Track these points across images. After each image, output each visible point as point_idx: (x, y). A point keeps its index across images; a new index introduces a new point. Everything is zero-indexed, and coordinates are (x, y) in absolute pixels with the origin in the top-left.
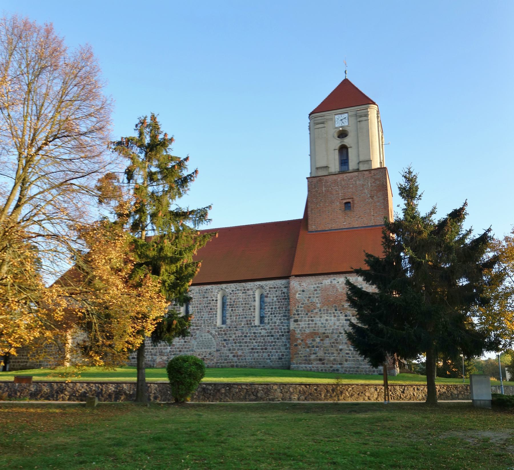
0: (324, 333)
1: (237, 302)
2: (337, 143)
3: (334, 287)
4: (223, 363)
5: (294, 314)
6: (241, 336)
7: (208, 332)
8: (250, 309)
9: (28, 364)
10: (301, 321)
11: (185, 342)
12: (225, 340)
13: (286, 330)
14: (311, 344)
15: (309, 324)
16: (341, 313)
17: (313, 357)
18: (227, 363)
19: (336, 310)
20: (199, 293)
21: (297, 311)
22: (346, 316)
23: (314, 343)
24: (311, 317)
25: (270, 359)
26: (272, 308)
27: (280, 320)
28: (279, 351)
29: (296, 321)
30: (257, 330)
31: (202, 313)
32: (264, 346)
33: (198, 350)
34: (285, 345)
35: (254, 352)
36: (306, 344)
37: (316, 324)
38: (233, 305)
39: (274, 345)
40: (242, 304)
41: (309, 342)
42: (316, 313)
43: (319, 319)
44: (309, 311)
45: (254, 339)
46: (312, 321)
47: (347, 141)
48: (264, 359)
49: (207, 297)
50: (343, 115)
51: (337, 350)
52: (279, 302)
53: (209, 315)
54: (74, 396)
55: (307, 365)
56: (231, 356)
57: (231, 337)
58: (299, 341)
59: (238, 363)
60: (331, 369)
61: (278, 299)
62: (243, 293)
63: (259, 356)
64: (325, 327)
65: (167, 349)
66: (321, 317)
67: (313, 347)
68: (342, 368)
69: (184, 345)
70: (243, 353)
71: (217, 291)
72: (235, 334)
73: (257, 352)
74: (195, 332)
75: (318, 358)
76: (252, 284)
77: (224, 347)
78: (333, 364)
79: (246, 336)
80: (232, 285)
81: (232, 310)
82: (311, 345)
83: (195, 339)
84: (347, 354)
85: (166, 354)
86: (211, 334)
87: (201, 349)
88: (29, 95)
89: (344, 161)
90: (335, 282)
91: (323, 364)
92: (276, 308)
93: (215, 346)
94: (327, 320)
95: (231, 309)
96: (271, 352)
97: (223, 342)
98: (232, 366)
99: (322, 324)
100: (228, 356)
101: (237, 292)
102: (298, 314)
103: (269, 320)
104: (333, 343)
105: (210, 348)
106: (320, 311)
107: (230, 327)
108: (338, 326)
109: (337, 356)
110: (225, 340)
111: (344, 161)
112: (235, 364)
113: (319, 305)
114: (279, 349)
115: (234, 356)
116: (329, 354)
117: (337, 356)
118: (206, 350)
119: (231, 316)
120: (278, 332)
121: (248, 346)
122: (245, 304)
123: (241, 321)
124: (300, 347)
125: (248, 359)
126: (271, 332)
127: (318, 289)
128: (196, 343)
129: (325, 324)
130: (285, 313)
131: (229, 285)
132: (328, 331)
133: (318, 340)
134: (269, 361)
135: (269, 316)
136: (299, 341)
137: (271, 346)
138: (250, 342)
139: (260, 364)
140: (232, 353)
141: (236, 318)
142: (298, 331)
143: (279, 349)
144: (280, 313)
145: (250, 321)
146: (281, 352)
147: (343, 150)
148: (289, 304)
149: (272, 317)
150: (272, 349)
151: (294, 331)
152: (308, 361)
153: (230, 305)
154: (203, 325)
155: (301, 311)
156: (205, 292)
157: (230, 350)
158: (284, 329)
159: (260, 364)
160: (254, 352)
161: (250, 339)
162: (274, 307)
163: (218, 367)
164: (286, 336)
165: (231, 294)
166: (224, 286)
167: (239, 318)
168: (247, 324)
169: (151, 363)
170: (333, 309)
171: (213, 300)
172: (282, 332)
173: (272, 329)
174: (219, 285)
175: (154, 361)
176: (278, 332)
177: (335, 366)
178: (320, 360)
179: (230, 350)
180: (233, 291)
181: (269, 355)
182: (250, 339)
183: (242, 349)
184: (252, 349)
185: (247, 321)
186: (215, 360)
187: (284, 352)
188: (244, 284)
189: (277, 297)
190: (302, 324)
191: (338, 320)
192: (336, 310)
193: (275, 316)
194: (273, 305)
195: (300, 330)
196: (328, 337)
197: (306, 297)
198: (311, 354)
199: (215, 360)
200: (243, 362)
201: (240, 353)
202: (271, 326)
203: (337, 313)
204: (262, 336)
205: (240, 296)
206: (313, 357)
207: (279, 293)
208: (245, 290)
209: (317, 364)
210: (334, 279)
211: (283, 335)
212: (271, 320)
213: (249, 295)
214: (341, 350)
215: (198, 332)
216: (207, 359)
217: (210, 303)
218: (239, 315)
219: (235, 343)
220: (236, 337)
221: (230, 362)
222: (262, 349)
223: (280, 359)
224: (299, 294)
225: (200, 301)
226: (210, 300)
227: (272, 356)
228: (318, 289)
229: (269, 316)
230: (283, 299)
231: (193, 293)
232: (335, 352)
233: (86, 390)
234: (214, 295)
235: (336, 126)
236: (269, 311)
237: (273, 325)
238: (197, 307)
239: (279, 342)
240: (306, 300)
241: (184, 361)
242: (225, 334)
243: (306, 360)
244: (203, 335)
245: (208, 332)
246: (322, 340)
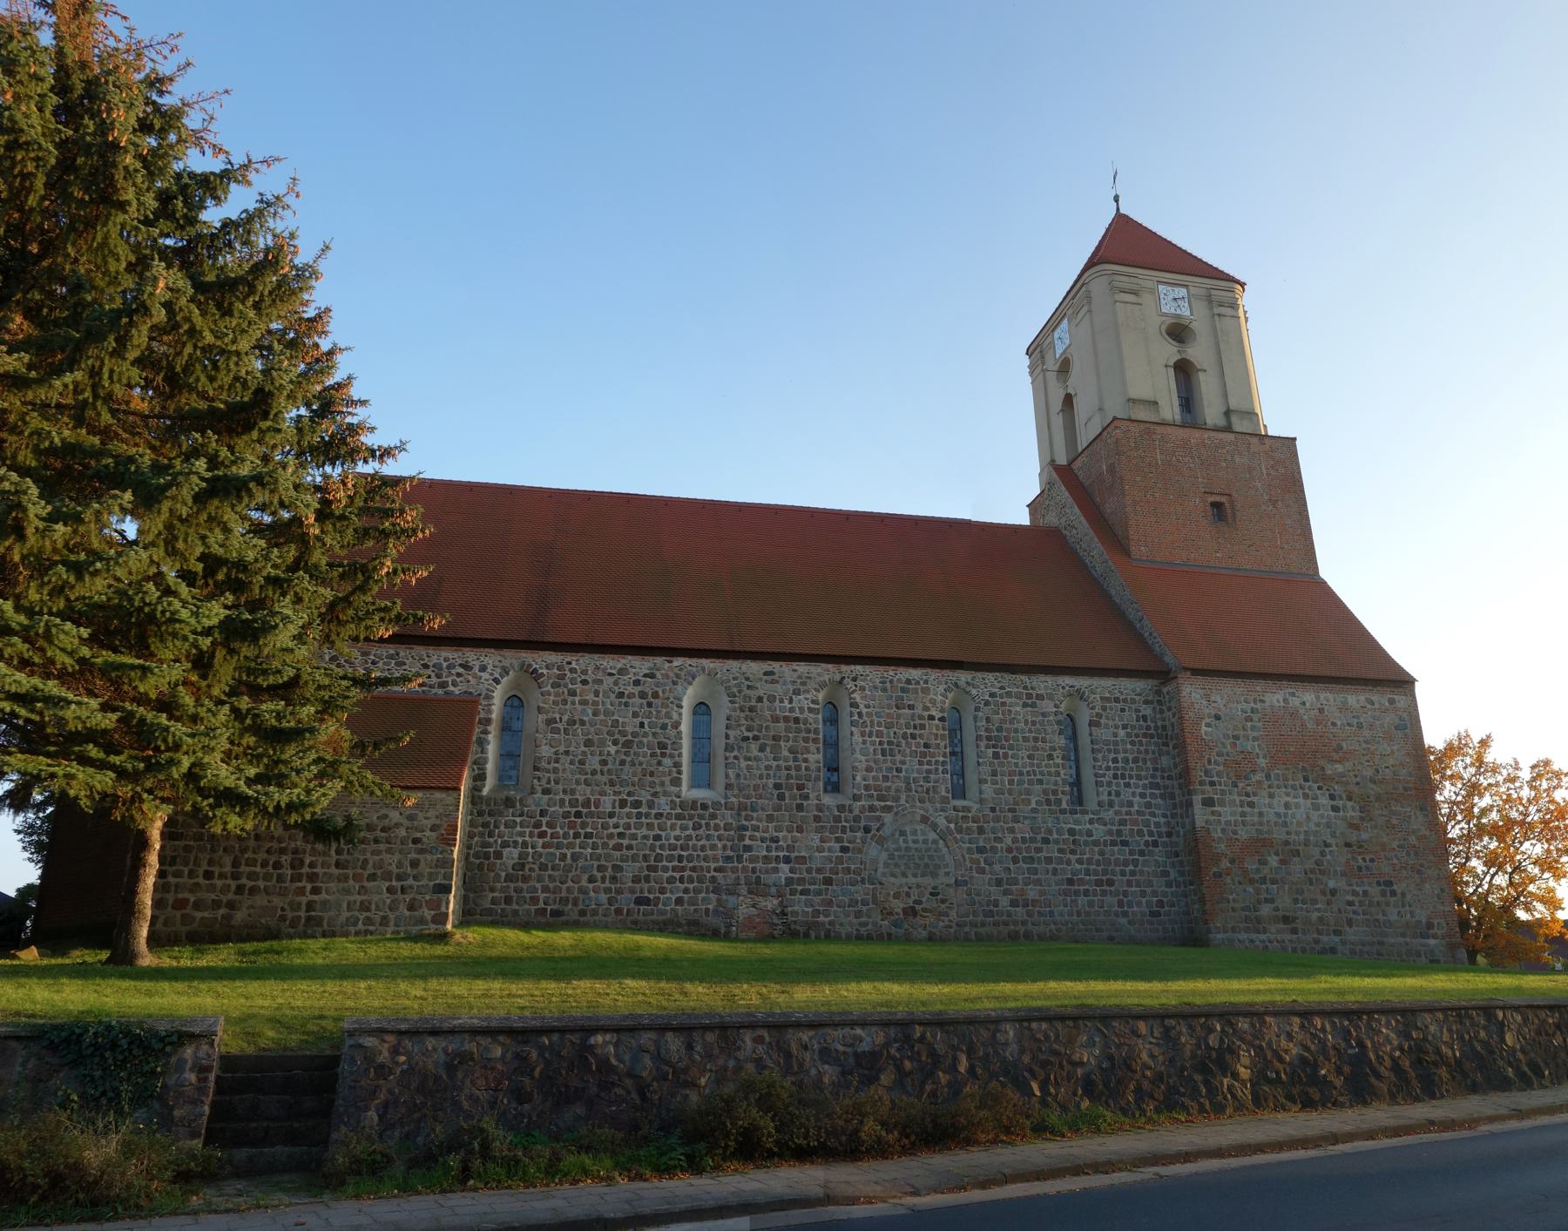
0: (1287, 843)
1: (1008, 730)
2: (1169, 352)
3: (1294, 714)
4: (983, 924)
5: (1202, 783)
6: (1033, 840)
7: (925, 820)
8: (1050, 757)
9: (240, 916)
10: (1222, 804)
11: (844, 850)
12: (981, 850)
13: (1164, 829)
14: (1258, 871)
15: (1243, 814)
16: (1320, 788)
17: (1266, 910)
18: (996, 924)
19: (1306, 780)
20: (884, 690)
21: (1207, 773)
22: (1332, 797)
23: (1266, 871)
24: (1248, 795)
25: (1125, 914)
26: (1115, 760)
27: (1142, 795)
28: (1149, 890)
29: (1208, 802)
30: (1077, 822)
31: (898, 757)
32: (1105, 872)
33: (892, 880)
34: (1165, 874)
35: (1077, 893)
36: (1245, 872)
37: (1261, 814)
38: (998, 739)
39: (1133, 873)
40: (1025, 739)
41: (1251, 866)
42: (1259, 782)
43: (1267, 801)
44: (1238, 777)
45: (1073, 852)
46: (1251, 805)
48: (1107, 913)
49: (911, 707)
51: (1323, 893)
52: (1133, 743)
53: (921, 763)
54: (1269, 1081)
55: (1254, 936)
56: (1004, 901)
57: (997, 839)
58: (1225, 864)
59: (1030, 927)
60: (1318, 947)
61: (1129, 735)
62: (1025, 705)
63: (1091, 904)
64: (1285, 824)
65: (776, 870)
66: (1271, 796)
67: (1263, 880)
68: (1343, 943)
69: (840, 860)
70: (1042, 893)
71: (941, 689)
72: (1012, 830)
73: (1086, 893)
74: (878, 819)
75: (1280, 913)
76: (1050, 680)
77: (982, 871)
78: (1319, 932)
79: (1046, 841)
80: (990, 677)
81: (996, 755)
82: (1257, 877)
83: (881, 841)
84: (1350, 903)
85: (773, 890)
86: (934, 827)
87: (904, 875)
89: (1188, 401)
90: (1295, 702)
91: (1294, 931)
92: (1126, 761)
93: (951, 869)
94: (1287, 806)
95: (990, 751)
96: (1125, 894)
97: (976, 856)
98: (1013, 937)
99: (1278, 815)
100: (996, 904)
101: (1008, 701)
102: (1212, 784)
103: (1110, 794)
104: (1312, 871)
105: (934, 875)
106: (1268, 777)
107: (993, 810)
108: (1318, 825)
109: (1326, 911)
110: (981, 850)
111: (1188, 401)
112: (1022, 929)
113: (1262, 762)
114: (1150, 884)
115: (1014, 903)
116: (1304, 902)
117: (1326, 911)
118: (920, 880)
119: (994, 774)
120: (1140, 833)
121: (1055, 872)
122: (1036, 740)
123: (1028, 792)
124: (1228, 880)
125: (1061, 914)
126: (1119, 833)
127: (1255, 717)
128: (884, 855)
129: (1286, 815)
130: (1153, 777)
131: (979, 675)
132: (1293, 837)
133: (1273, 861)
134: (1123, 921)
135: (1109, 784)
136: (1225, 864)
137: (1123, 874)
138: (1060, 861)
139: (1097, 930)
140: (1006, 893)
141: (1011, 782)
142: (1217, 834)
143: (1150, 884)
144: (1139, 777)
145: (1055, 792)
146: (1155, 893)
147: (1184, 370)
149: (1118, 785)
150: (1129, 883)
151: (1208, 831)
152: (1256, 925)
153: (989, 738)
154: (903, 797)
155: (1219, 774)
156: (903, 690)
157: (999, 882)
158: (1157, 825)
159: (1097, 930)
160: (1077, 893)
161: (1061, 851)
162: (1120, 756)
163: (967, 939)
164: (1165, 844)
165: (987, 703)
166: (963, 677)
167: (1020, 783)
168: (1048, 802)
169: (713, 921)
170: (1300, 775)
171: (931, 718)
172: (1151, 834)
173: (1123, 823)
174: (947, 672)
175: (728, 914)
176: (1140, 833)
177: (1325, 938)
178: (1286, 919)
179: (999, 882)
180: (992, 695)
181: (1121, 904)
182: (1061, 851)
183: (1038, 882)
184: (1070, 882)
185: (1045, 792)
186: (953, 914)
187: (1165, 894)
188: (1024, 678)
189: (1125, 727)
190: (1227, 813)
191: (1316, 807)
192: (1306, 780)
193: (1127, 785)
194: (1116, 752)
195: (1223, 830)
196: (1297, 853)
197: (1226, 736)
198: (1259, 902)
199: (953, 914)
200: (1045, 923)
201: (1032, 893)
202: (1116, 813)
203: (1310, 788)
204: (1096, 843)
205: (1017, 713)
206: (1266, 910)
207: (1129, 717)
208: (1029, 696)
209: (1278, 932)
210: (1293, 694)
211: (1155, 844)
212: (1118, 794)
213: (1043, 715)
214: (1333, 892)
215: (888, 818)
216: (924, 910)
217: (923, 727)
218: (1021, 774)
219: (1015, 860)
220: (1015, 840)
221: (1006, 924)
222: (1099, 883)
223: (1152, 914)
224: (1208, 725)
225: (889, 715)
226: (921, 717)
227: (1130, 905)
228: (1255, 717)
229: (1109, 784)
230: (1145, 735)
231: (863, 689)
232: (1320, 898)
233: (1306, 1048)
234: (933, 702)
236: (1108, 768)
237: (1124, 810)
238: (879, 734)
239: (1145, 863)
240: (1228, 742)
242: (981, 831)
243: (1247, 919)
244: (908, 829)
245: (925, 820)
246: (1283, 862)
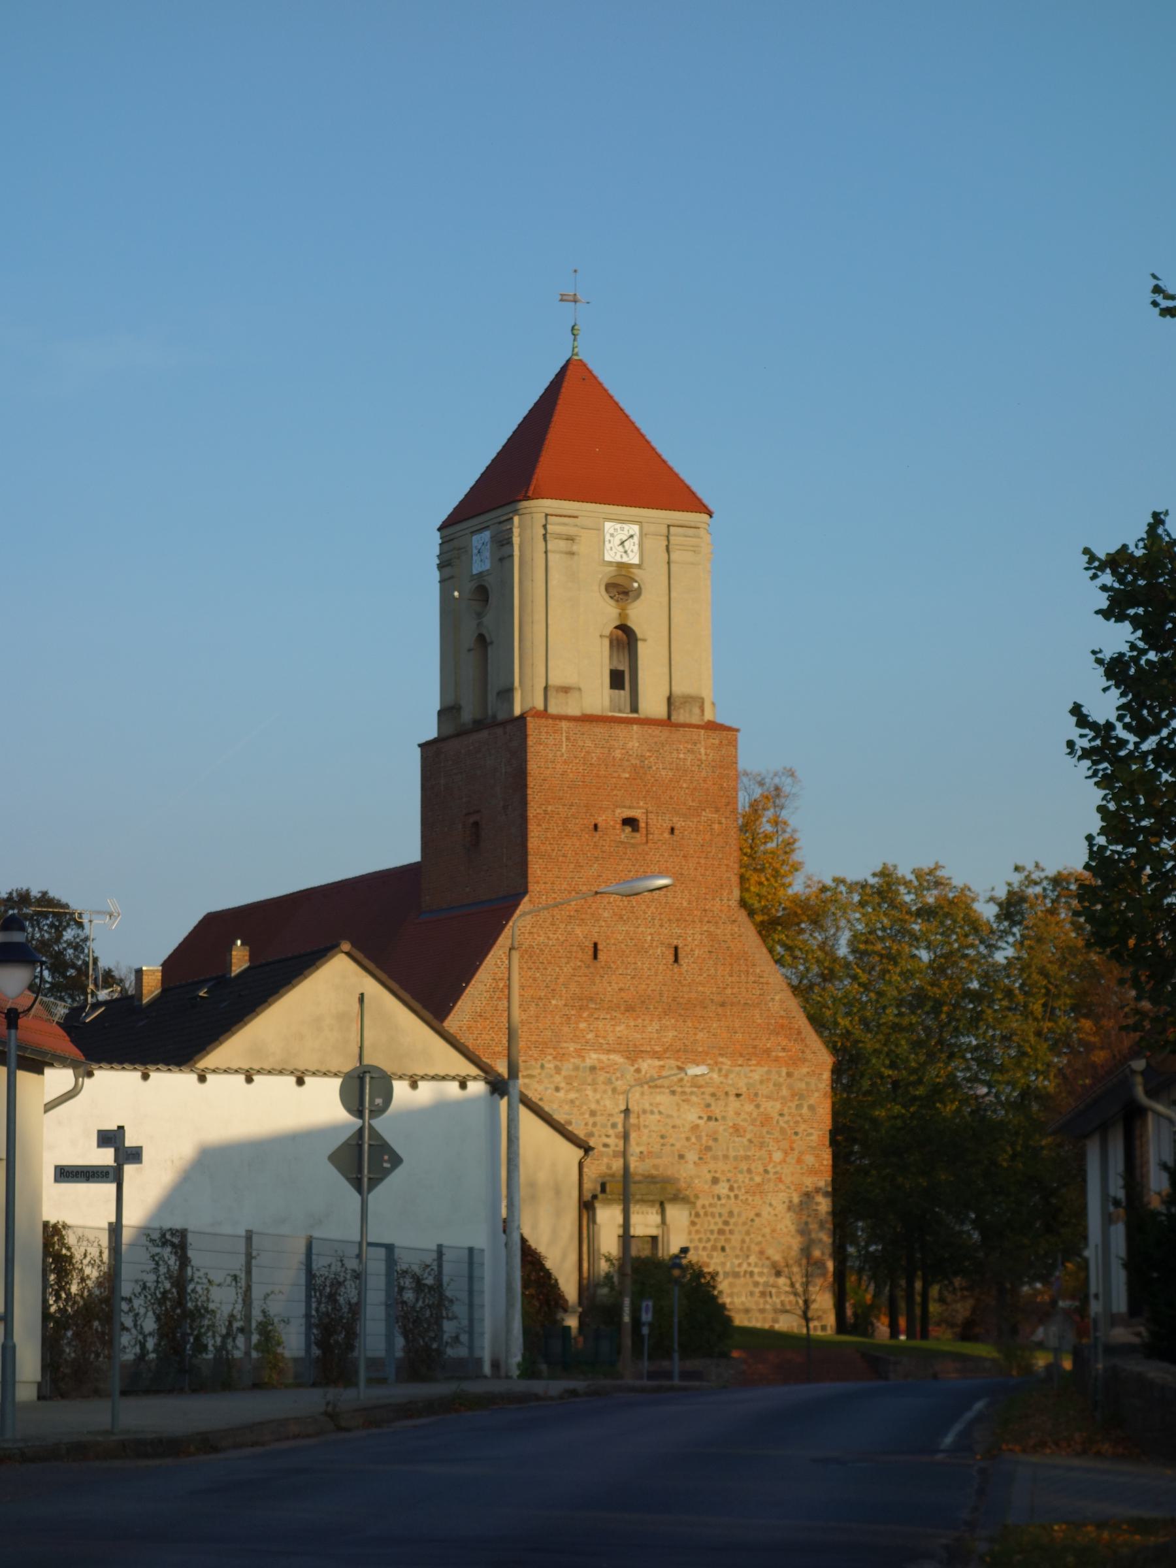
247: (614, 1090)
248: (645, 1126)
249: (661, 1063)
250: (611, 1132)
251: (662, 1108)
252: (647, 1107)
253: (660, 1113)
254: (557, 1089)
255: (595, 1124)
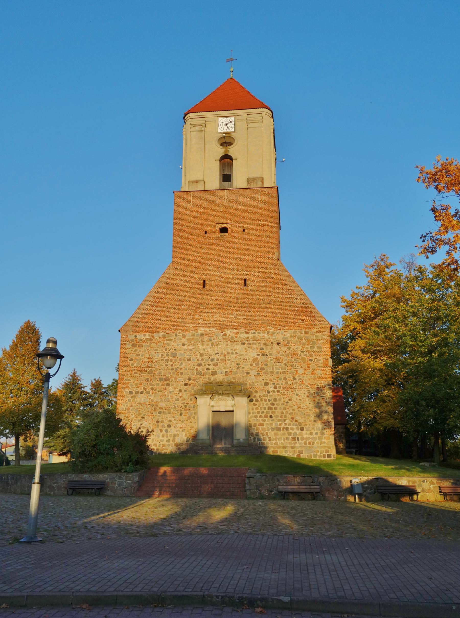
47: (232, 151)
50: (228, 119)
88: (55, 474)
111: (227, 178)
147: (226, 160)
148: (160, 534)
235: (219, 131)
241: (311, 313)
247: (212, 344)
248: (229, 360)
249: (237, 331)
250: (211, 363)
251: (237, 351)
252: (230, 351)
253: (236, 353)
254: (183, 345)
255: (202, 360)
